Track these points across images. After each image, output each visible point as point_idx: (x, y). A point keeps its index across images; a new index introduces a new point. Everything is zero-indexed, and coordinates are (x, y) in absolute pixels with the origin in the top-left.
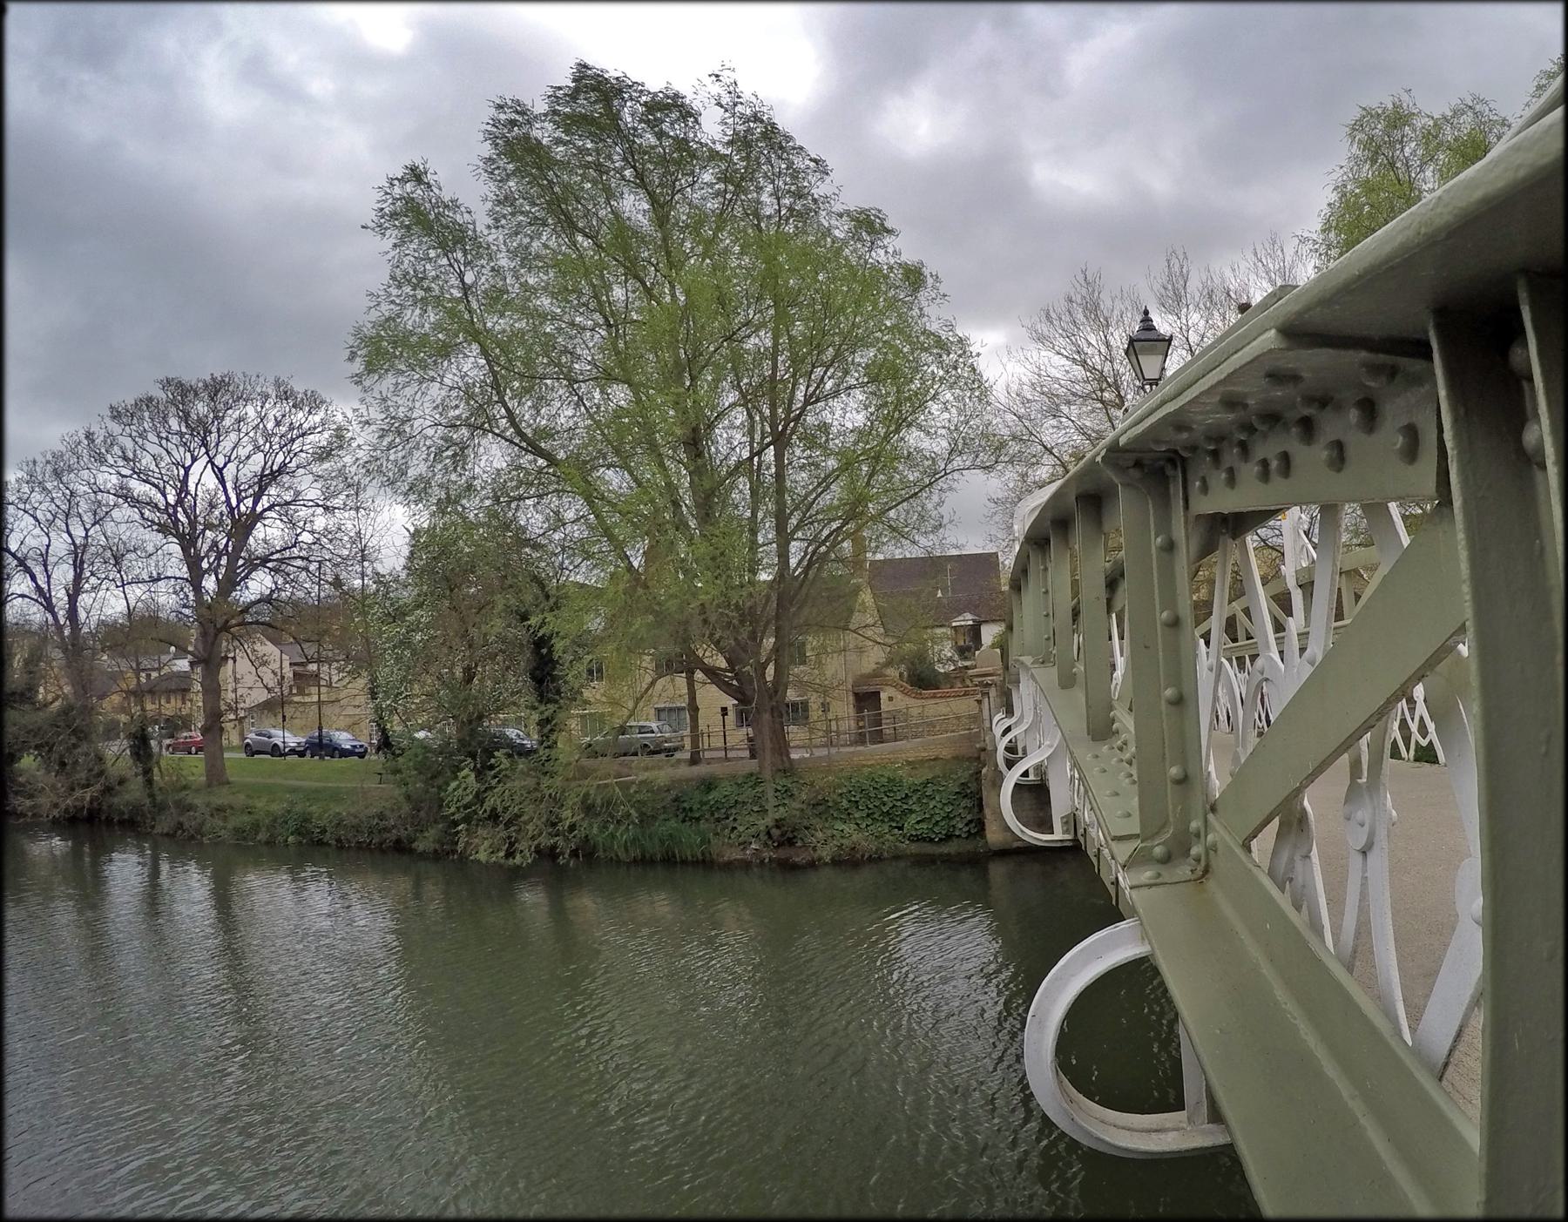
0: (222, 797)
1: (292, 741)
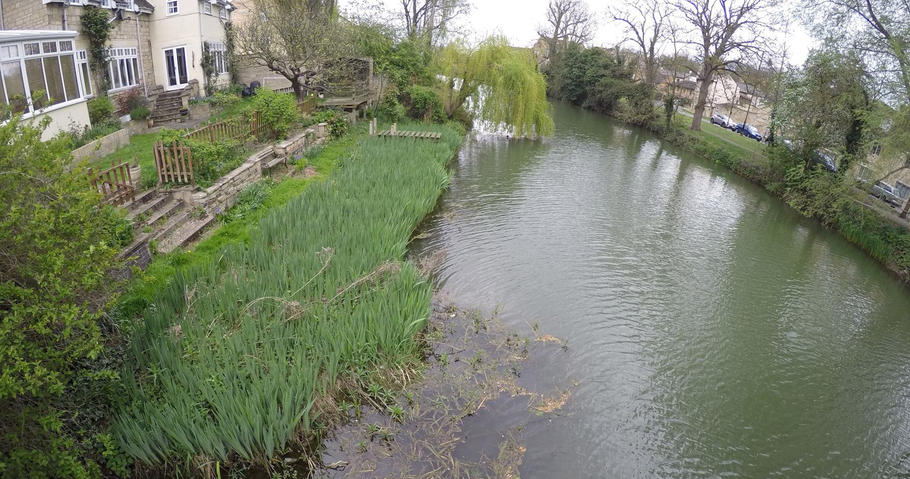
0: (695, 135)
1: (732, 123)
